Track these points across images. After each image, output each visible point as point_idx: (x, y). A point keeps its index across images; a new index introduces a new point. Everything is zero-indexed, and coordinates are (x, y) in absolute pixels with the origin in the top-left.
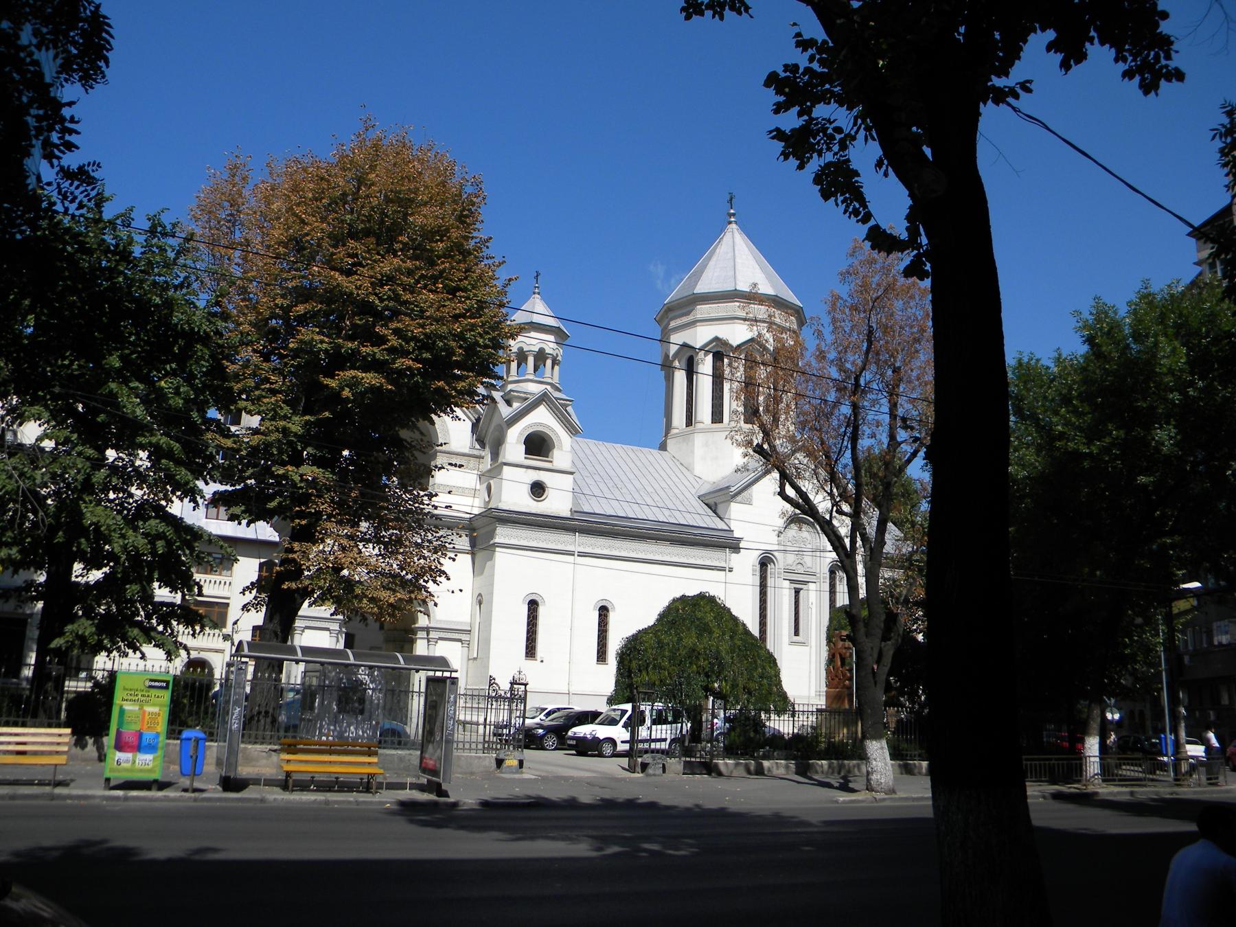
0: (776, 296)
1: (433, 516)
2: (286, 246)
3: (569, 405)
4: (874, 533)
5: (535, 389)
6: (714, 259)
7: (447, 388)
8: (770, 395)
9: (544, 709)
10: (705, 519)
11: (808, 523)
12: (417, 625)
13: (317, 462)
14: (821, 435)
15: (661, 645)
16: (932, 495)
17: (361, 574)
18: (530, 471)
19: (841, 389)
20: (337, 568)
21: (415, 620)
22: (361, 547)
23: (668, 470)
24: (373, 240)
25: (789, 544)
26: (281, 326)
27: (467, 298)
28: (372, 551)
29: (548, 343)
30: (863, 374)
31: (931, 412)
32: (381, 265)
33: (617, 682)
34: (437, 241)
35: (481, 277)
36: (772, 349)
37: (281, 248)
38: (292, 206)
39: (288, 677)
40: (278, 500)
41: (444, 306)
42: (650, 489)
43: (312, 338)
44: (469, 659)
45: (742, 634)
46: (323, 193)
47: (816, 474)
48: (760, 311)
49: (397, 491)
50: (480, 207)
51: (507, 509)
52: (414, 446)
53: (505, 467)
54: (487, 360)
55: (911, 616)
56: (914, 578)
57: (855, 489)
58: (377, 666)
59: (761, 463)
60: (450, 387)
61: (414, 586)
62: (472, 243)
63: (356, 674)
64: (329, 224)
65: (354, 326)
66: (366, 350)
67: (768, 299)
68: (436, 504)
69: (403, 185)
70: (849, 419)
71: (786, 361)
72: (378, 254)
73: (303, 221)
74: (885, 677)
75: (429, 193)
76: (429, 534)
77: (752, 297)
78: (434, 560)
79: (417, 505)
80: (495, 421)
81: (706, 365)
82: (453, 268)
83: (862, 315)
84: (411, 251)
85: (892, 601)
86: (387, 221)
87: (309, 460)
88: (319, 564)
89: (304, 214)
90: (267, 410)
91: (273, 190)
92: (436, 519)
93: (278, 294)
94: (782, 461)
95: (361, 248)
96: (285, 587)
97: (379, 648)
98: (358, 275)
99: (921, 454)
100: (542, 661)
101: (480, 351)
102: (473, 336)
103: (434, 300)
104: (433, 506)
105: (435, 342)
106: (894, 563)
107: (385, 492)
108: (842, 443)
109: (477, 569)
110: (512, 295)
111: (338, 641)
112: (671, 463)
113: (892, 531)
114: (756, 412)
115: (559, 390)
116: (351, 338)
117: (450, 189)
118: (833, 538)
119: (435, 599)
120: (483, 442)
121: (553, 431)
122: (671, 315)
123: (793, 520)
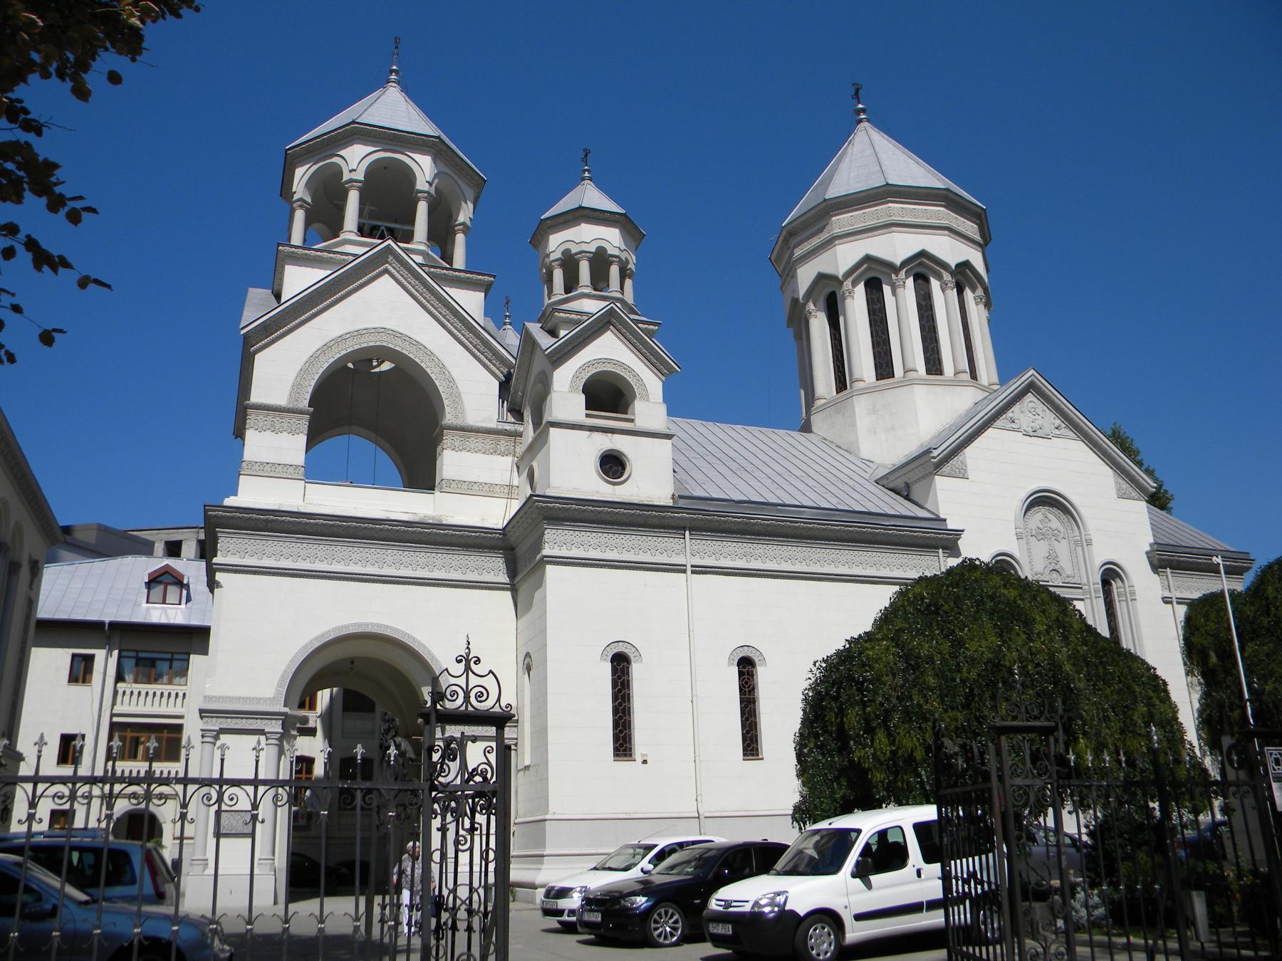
5: (592, 306)
9: (649, 848)
15: (912, 662)
23: (821, 453)
53: (552, 430)
81: (856, 306)
100: (645, 762)
112: (821, 445)
121: (627, 368)
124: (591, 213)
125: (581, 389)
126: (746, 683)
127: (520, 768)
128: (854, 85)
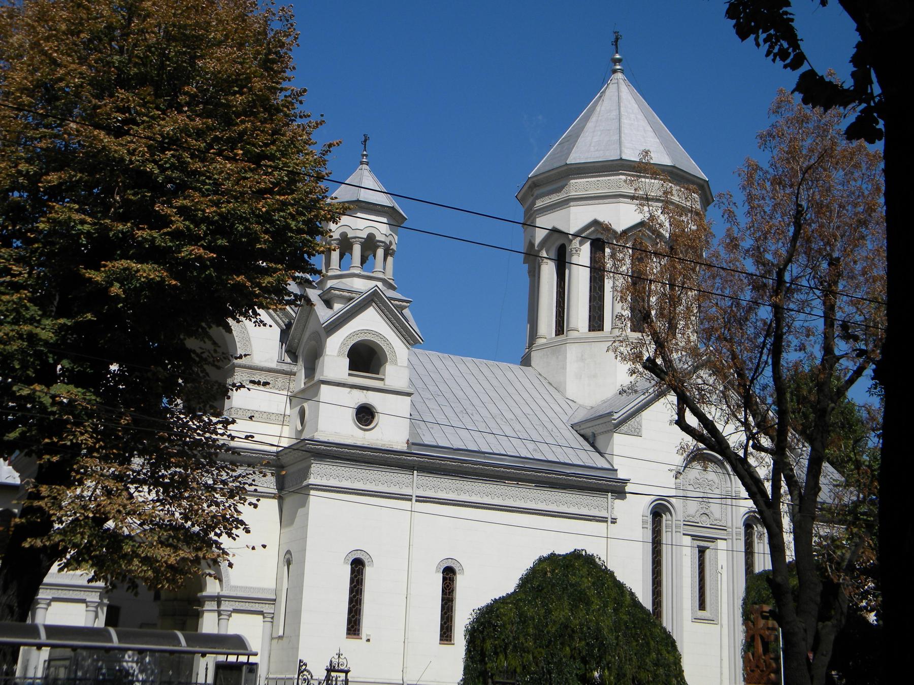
0: (674, 167)
1: (229, 449)
2: (30, 93)
3: (406, 307)
4: (804, 476)
5: (362, 286)
6: (594, 119)
7: (248, 284)
8: (665, 294)
10: (583, 456)
11: (720, 464)
12: (204, 594)
13: (73, 379)
14: (731, 347)
15: (523, 619)
16: (885, 426)
17: (132, 526)
18: (355, 391)
19: (758, 287)
20: (100, 518)
21: (202, 586)
22: (132, 491)
24: (150, 90)
25: (690, 488)
26: (26, 201)
27: (276, 168)
28: (147, 495)
29: (380, 228)
30: (789, 268)
31: (881, 318)
32: (162, 122)
33: (467, 669)
34: (235, 93)
35: (292, 141)
36: (667, 235)
37: (24, 97)
38: (38, 41)
39: (25, 668)
40: (20, 428)
41: (245, 178)
42: (509, 415)
43: (70, 218)
44: (272, 639)
45: (629, 606)
46: (82, 25)
47: (725, 397)
48: (653, 186)
49: (182, 416)
50: (290, 50)
51: (326, 440)
52: (205, 360)
54: (301, 249)
55: (858, 588)
56: (860, 537)
57: (779, 418)
58: (151, 651)
59: (653, 382)
60: (252, 283)
61: (203, 542)
62: (281, 96)
63: (120, 661)
64: (90, 66)
65: (126, 202)
66: (142, 234)
67: (663, 171)
68: (234, 434)
69: (188, 18)
70: (770, 325)
71: (686, 251)
72: (158, 108)
73: (54, 62)
74: (825, 669)
75: (223, 30)
76: (223, 473)
77: (641, 168)
78: (230, 506)
79: (207, 435)
80: (311, 327)
81: (582, 255)
82: (255, 129)
83: (788, 191)
84: (201, 106)
85: (831, 567)
86: (169, 66)
87: (64, 376)
88: (75, 513)
89: (56, 51)
90: (7, 310)
91: (11, 16)
92: (233, 453)
93: (22, 158)
94: (680, 380)
95: (134, 100)
96: (26, 545)
97: (154, 625)
98: (130, 135)
99: (869, 371)
100: (368, 640)
101: (291, 237)
102: (283, 217)
103: (232, 170)
104: (228, 436)
105: (233, 224)
106: (833, 516)
107: (166, 418)
108: (761, 357)
109: (286, 518)
110: (332, 166)
111: (96, 616)
112: (536, 383)
113: (829, 474)
114: (646, 317)
115: (391, 287)
116: (123, 219)
117: (252, 25)
118: (749, 481)
119: (230, 558)
120: (295, 353)
122: (537, 192)
123: (694, 457)
124: (367, 206)
125: (347, 353)
126: (448, 586)
127: (275, 635)
128: (615, 33)
